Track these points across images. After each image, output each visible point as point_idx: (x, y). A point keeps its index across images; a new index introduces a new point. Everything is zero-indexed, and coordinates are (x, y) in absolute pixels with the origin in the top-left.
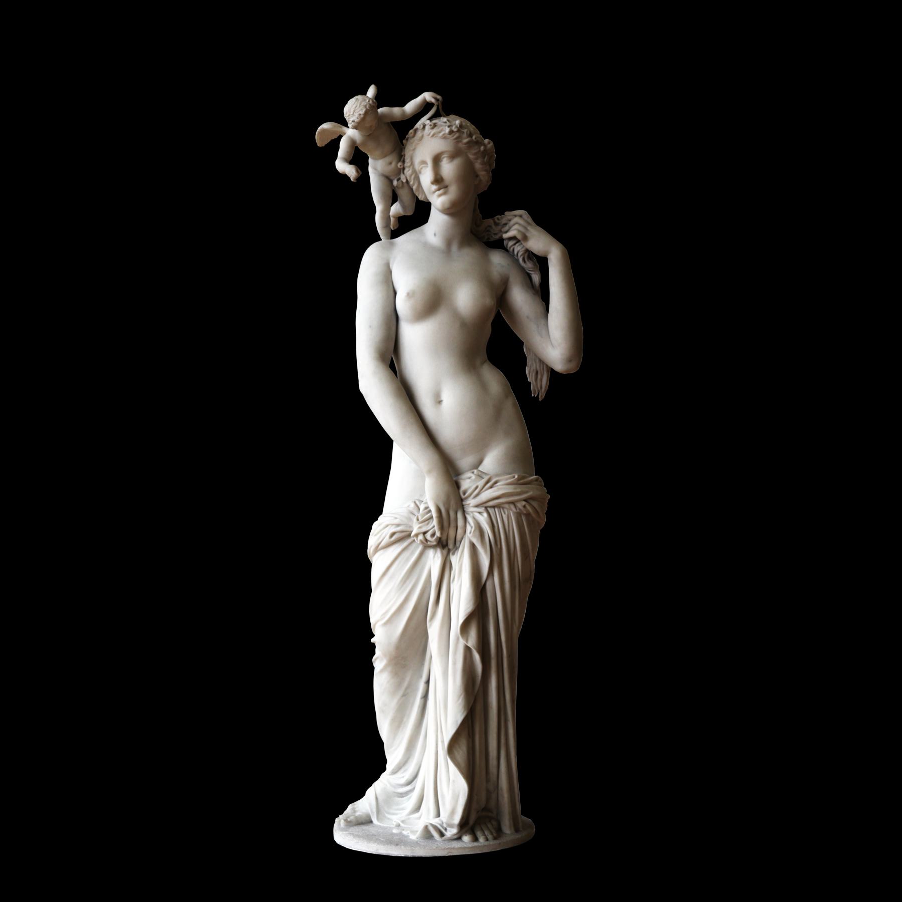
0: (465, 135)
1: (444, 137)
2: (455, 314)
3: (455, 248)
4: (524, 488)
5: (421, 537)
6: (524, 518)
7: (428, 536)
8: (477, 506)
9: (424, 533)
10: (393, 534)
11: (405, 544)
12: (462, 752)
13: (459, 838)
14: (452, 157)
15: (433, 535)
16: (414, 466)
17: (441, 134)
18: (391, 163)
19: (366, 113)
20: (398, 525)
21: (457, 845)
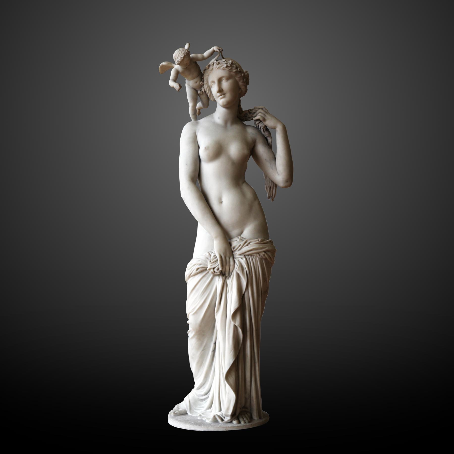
0: (234, 68)
1: (223, 69)
2: (229, 158)
3: (229, 125)
4: (264, 246)
5: (212, 270)
6: (263, 261)
7: (216, 270)
8: (240, 255)
9: (214, 268)
10: (198, 269)
11: (204, 274)
12: (232, 379)
13: (231, 422)
14: (228, 79)
15: (218, 269)
16: (208, 234)
17: (222, 68)
18: (197, 82)
19: (184, 57)
20: (200, 264)
21: (230, 425)
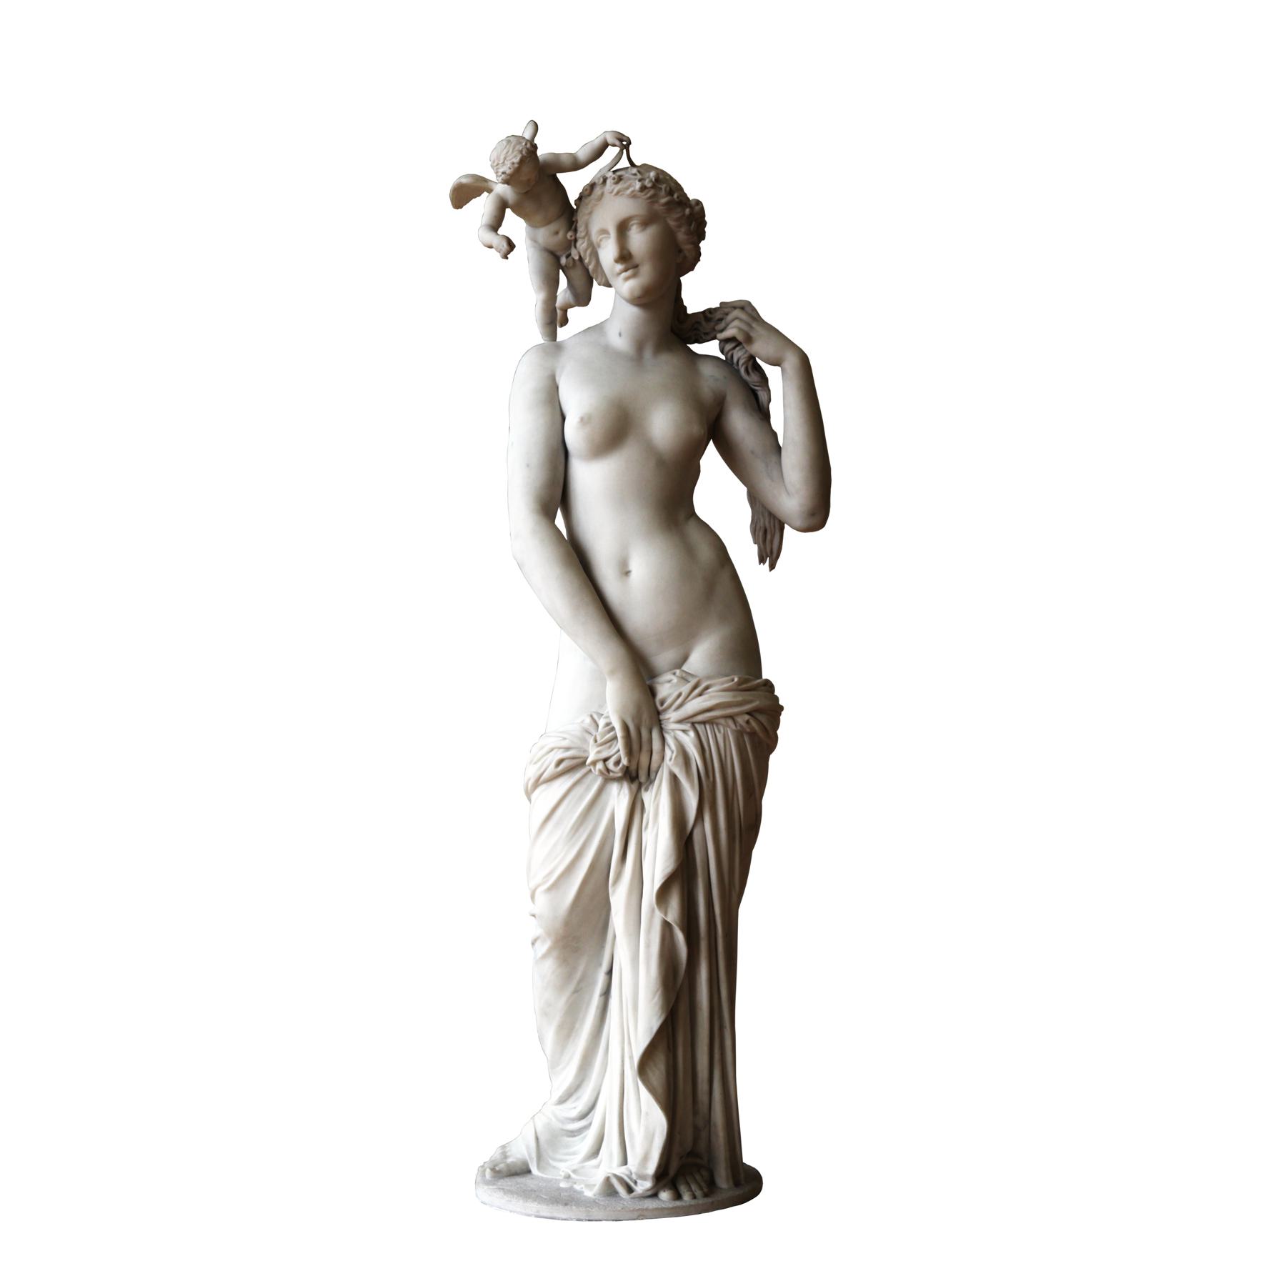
0: (663, 193)
1: (633, 196)
2: (649, 448)
3: (648, 353)
4: (747, 695)
5: (600, 766)
6: (746, 739)
7: (610, 764)
8: (680, 722)
9: (605, 760)
10: (560, 762)
11: (578, 775)
12: (658, 1073)
14: (645, 224)
15: (617, 763)
20: (568, 749)
